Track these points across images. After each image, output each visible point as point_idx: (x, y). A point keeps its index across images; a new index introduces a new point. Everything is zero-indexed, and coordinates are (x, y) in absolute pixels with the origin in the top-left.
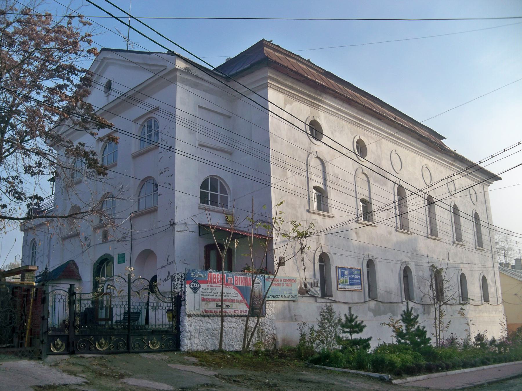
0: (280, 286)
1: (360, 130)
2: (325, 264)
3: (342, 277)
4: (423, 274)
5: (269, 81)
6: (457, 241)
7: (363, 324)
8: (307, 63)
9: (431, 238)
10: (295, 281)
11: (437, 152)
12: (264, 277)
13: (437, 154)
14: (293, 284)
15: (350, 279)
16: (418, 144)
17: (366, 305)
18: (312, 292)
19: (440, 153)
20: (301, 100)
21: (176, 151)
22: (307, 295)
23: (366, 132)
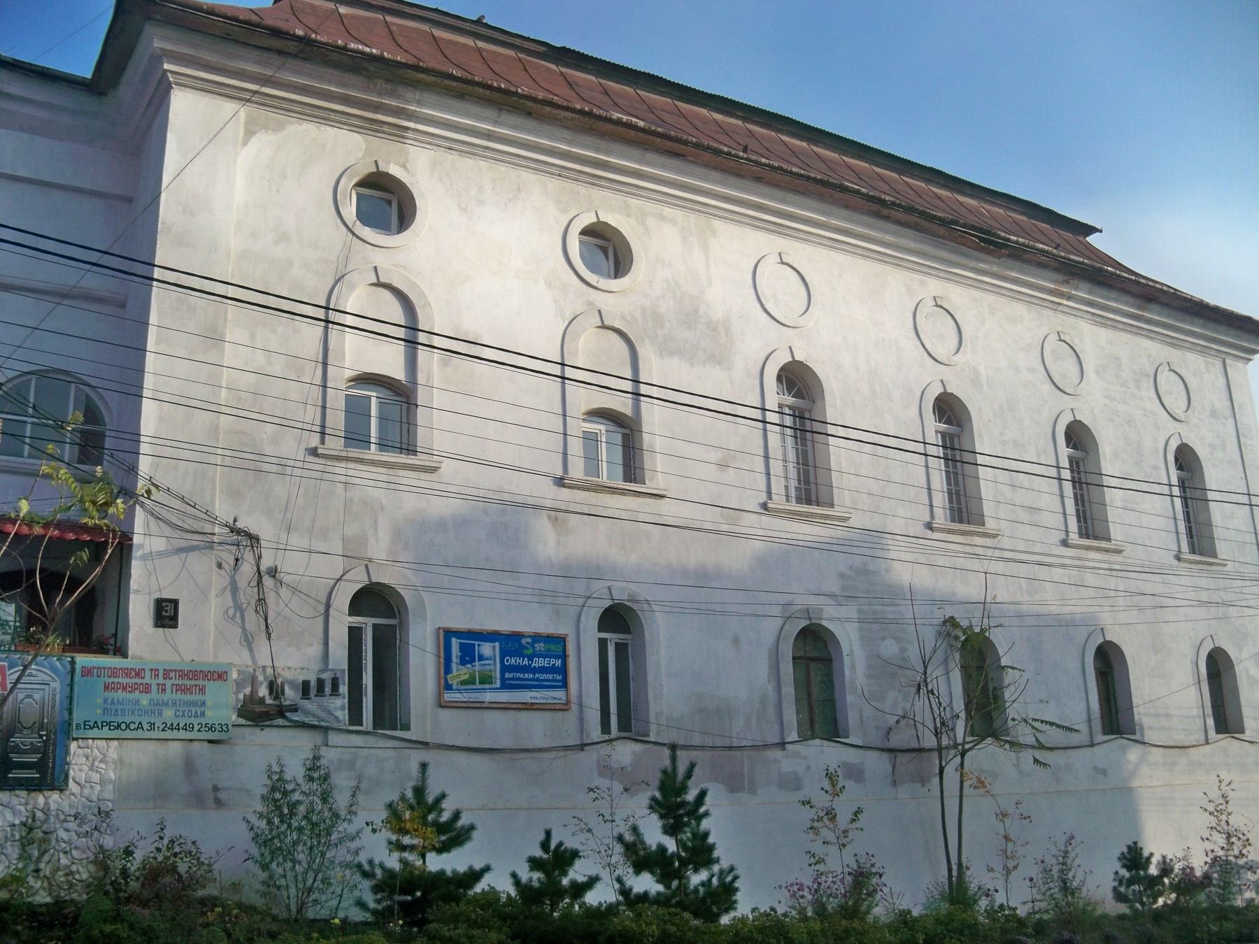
0: (147, 689)
1: (599, 195)
2: (401, 624)
3: (463, 662)
4: (903, 650)
5: (166, 66)
6: (1193, 551)
7: (463, 821)
8: (475, 28)
9: (1191, 562)
10: (221, 676)
11: (976, 253)
12: (73, 663)
13: (978, 260)
14: (211, 686)
15: (504, 669)
16: (887, 232)
17: (591, 756)
18: (306, 713)
19: (991, 258)
20: (324, 117)
21: (980, 460)
22: (281, 721)
23: (634, 202)
